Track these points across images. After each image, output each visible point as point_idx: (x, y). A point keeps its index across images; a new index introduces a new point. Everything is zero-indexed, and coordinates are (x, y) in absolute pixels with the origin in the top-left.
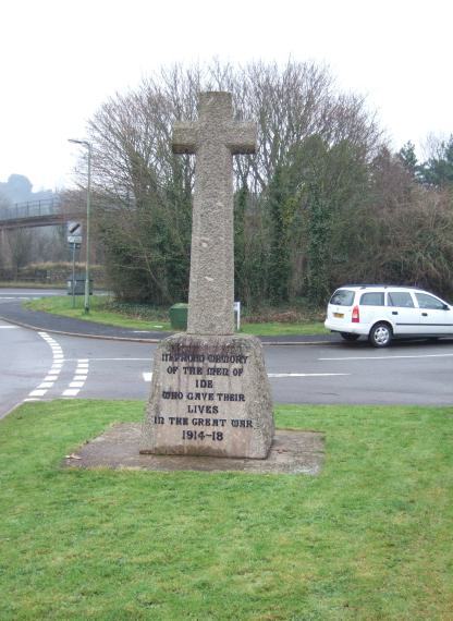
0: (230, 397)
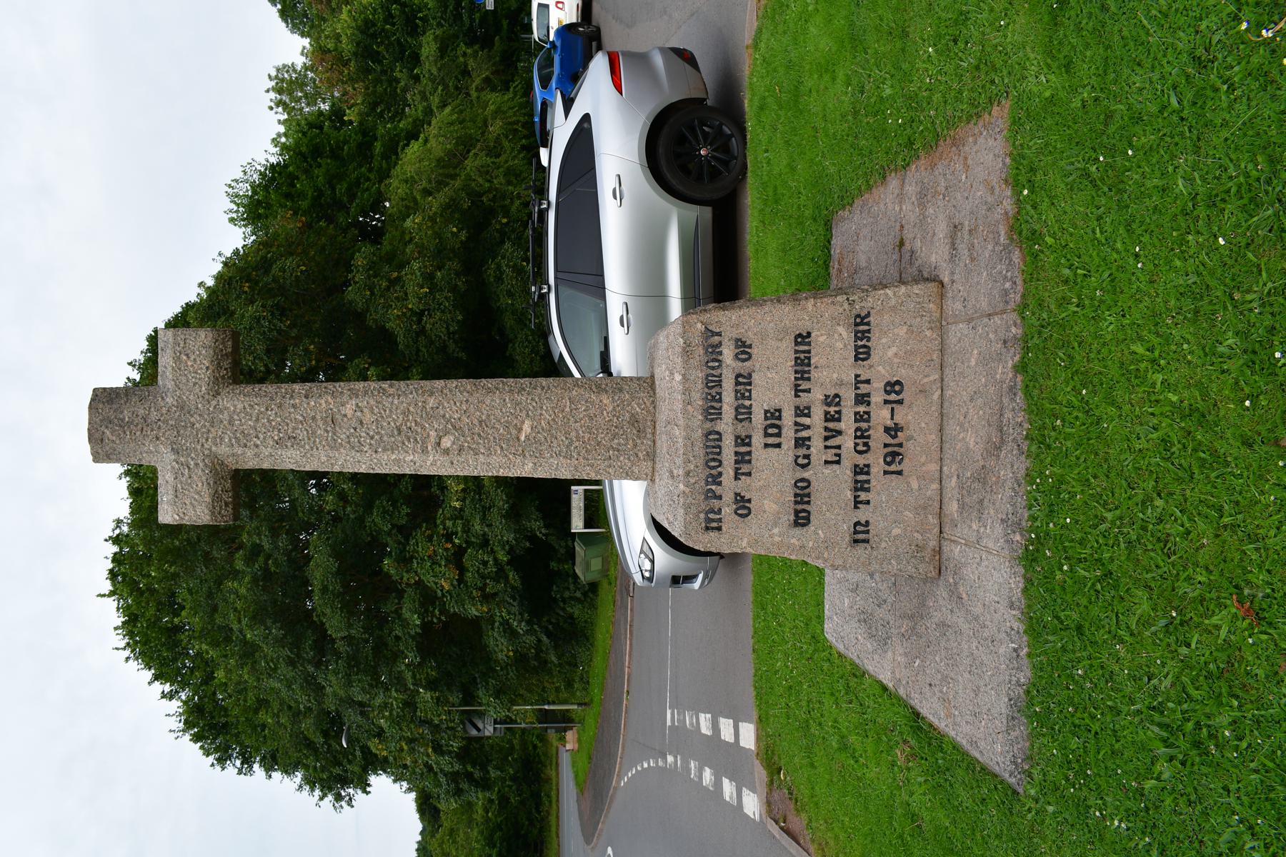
0: (803, 366)
